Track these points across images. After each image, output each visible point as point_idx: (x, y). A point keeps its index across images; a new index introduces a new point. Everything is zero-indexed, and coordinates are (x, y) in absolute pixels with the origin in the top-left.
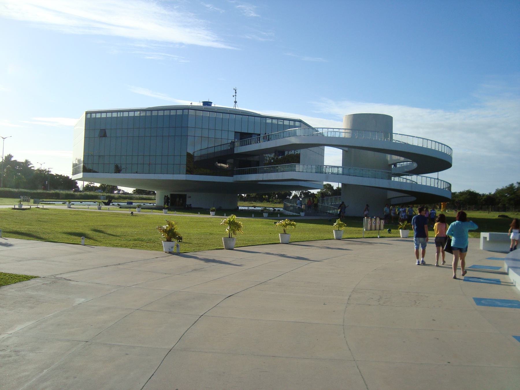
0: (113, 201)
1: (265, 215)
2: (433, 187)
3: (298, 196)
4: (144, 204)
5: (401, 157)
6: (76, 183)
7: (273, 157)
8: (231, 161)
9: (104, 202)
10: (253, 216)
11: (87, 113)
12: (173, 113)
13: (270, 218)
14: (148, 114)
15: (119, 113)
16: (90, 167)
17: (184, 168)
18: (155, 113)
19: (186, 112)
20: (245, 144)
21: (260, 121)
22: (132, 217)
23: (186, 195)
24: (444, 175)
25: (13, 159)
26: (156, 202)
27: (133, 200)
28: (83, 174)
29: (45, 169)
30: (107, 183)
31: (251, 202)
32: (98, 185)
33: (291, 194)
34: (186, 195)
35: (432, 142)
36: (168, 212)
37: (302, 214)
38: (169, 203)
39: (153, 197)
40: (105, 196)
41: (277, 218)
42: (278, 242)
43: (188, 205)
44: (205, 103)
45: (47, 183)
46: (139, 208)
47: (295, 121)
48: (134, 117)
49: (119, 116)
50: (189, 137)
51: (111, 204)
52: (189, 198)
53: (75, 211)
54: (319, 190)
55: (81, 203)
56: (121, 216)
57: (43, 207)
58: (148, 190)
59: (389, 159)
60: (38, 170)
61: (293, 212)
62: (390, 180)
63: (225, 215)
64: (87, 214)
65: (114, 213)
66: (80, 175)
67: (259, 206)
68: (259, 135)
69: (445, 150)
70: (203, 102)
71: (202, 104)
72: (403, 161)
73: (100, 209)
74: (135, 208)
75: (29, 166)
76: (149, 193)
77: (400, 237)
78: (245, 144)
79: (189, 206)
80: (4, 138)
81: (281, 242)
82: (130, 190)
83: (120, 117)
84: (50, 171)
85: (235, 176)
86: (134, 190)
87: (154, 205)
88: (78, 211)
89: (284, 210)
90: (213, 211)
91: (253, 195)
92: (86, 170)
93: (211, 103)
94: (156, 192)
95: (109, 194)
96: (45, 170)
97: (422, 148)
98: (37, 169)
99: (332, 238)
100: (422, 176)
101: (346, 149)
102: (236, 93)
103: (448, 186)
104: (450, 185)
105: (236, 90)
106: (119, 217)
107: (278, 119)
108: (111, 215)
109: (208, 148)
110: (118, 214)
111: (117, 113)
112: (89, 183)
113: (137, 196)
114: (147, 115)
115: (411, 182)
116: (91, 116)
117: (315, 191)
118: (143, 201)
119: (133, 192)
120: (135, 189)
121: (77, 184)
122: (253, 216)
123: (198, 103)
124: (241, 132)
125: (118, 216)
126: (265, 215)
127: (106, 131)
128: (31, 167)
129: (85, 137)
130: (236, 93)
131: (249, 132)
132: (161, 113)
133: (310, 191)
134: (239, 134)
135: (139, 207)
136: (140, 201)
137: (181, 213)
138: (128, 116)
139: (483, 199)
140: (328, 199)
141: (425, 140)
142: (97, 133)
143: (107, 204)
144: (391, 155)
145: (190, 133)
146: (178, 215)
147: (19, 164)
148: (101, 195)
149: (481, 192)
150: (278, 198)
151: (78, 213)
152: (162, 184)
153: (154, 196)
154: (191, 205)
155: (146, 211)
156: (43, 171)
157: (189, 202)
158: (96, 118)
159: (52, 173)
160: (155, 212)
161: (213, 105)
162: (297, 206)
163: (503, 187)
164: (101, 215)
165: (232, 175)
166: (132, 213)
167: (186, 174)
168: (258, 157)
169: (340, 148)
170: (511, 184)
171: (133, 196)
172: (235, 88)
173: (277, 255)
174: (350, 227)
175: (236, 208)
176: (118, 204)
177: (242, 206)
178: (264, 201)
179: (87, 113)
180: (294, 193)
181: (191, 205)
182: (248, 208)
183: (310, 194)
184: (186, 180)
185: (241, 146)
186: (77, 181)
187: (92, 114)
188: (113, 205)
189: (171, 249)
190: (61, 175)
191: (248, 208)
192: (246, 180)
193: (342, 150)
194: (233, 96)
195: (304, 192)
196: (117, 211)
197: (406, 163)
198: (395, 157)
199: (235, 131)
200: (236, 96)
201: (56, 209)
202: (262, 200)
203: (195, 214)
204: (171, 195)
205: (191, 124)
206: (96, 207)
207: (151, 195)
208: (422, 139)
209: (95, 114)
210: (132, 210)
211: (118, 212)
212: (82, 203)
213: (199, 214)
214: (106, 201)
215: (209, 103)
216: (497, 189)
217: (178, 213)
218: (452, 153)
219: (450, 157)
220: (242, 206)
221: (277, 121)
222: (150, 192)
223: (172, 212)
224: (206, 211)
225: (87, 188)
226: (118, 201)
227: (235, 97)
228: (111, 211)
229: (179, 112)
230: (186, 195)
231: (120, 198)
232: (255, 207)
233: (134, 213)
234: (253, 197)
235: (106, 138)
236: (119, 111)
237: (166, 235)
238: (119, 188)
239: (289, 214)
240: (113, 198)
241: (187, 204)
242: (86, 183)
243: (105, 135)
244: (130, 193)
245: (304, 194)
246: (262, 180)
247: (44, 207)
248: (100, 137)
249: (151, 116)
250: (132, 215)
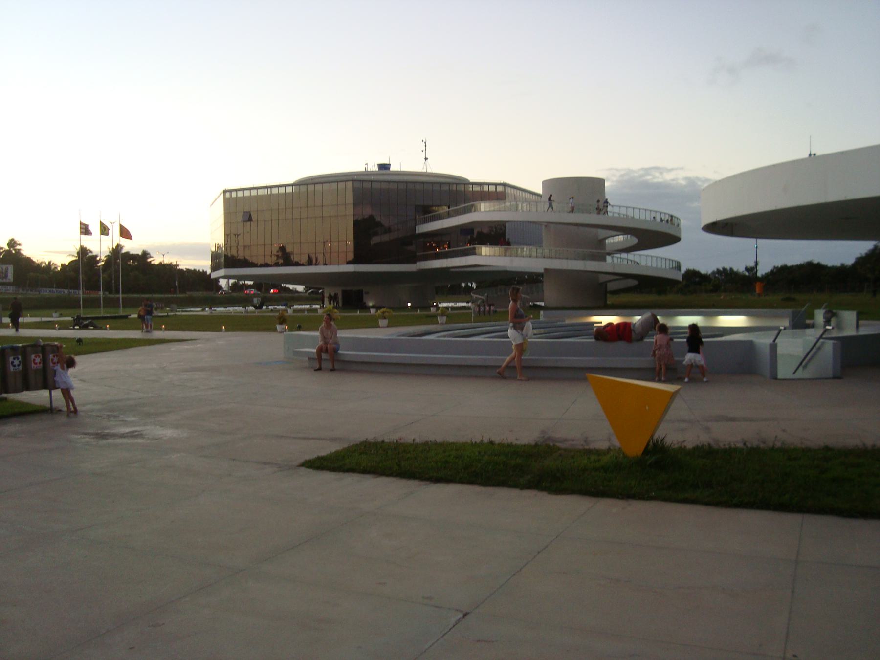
11: (225, 192)
25: (124, 251)
66: (222, 272)
75: (149, 260)
80: (113, 222)
85: (418, 263)
102: (426, 146)
105: (425, 143)
115: (619, 262)
116: (231, 195)
127: (252, 214)
128: (150, 262)
129: (225, 223)
130: (426, 146)
144: (20, 326)
147: (134, 257)
149: (830, 264)
159: (181, 267)
161: (392, 168)
163: (861, 254)
172: (424, 140)
215: (70, 401)
225: (235, 288)
243: (250, 219)
248: (244, 222)
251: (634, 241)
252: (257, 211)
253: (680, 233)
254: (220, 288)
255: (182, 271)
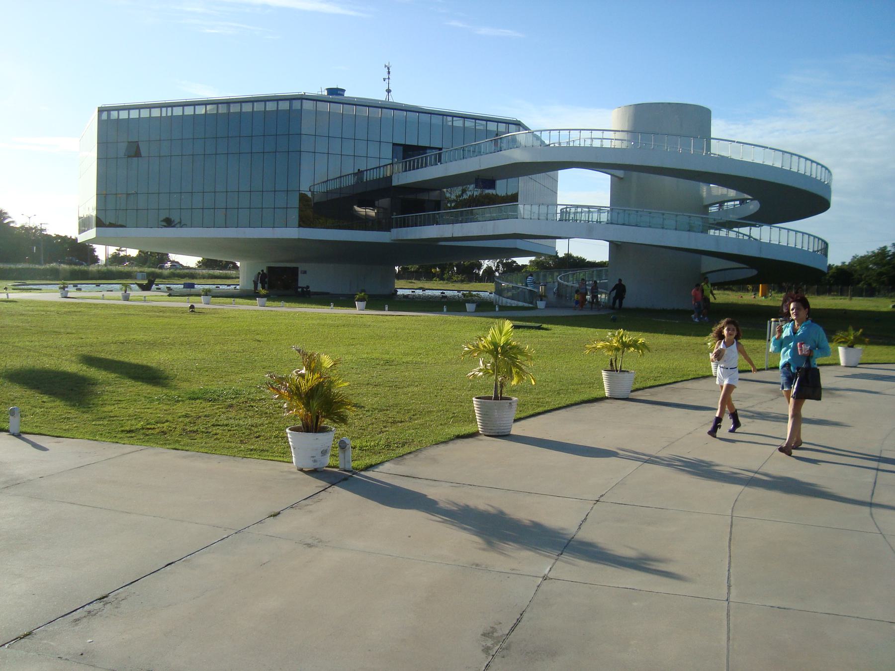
0: (157, 281)
1: (470, 307)
2: (800, 249)
3: (494, 269)
4: (216, 287)
5: (730, 190)
6: (93, 250)
7: (455, 198)
8: (385, 202)
9: (139, 285)
10: (445, 310)
11: (101, 111)
12: (271, 106)
13: (481, 314)
14: (222, 109)
15: (164, 110)
16: (111, 219)
17: (294, 215)
18: (234, 109)
19: (296, 105)
20: (414, 165)
21: (441, 123)
22: (193, 317)
23: (297, 268)
24: (811, 225)
26: (240, 283)
27: (196, 278)
28: (96, 230)
29: (35, 226)
30: (149, 250)
31: (410, 281)
32: (133, 253)
33: (479, 266)
34: (297, 268)
35: (791, 156)
36: (268, 303)
37: (541, 304)
38: (266, 285)
39: (233, 273)
40: (145, 274)
41: (492, 314)
42: (596, 394)
43: (302, 288)
44: (331, 91)
45: (35, 251)
46: (206, 295)
47: (509, 123)
48: (195, 116)
49: (164, 114)
50: (303, 154)
51: (154, 287)
52: (304, 273)
53: (73, 304)
54: (533, 258)
55: (97, 286)
56: (168, 314)
57: (8, 297)
58: (225, 259)
59: (705, 194)
60: (23, 227)
61: (519, 301)
62: (706, 235)
63: (387, 308)
64: (94, 311)
65: (155, 306)
67: (433, 289)
68: (440, 149)
69: (816, 173)
70: (327, 89)
71: (325, 93)
72: (734, 198)
73: (126, 298)
74: (200, 295)
75: (6, 221)
76: (225, 266)
77: (838, 364)
78: (414, 165)
79: (305, 289)
81: (607, 395)
82: (190, 261)
83: (167, 116)
84: (45, 230)
86: (199, 262)
87: (236, 287)
88: (79, 303)
89: (498, 296)
90: (360, 300)
91: (413, 268)
92: (100, 223)
93: (343, 91)
94: (238, 264)
95: (153, 269)
96: (36, 227)
97: (781, 170)
98: (20, 226)
99: (701, 373)
100: (780, 228)
101: (620, 173)
102: (389, 73)
103: (823, 247)
104: (826, 244)
105: (389, 69)
106: (162, 317)
107: (476, 119)
108: (147, 311)
109: (341, 177)
110: (163, 310)
111: (160, 109)
112: (117, 250)
113: (205, 272)
114: (220, 112)
116: (109, 115)
117: (522, 261)
118: (215, 280)
119: (197, 265)
120: (200, 259)
121: (95, 251)
122: (445, 310)
123: (317, 87)
124: (404, 143)
125: (161, 314)
126: (470, 307)
127: (141, 145)
128: (9, 223)
129: (99, 159)
130: (389, 73)
131: (421, 144)
132: (247, 108)
133: (514, 259)
134: (401, 148)
135: (207, 293)
136: (210, 281)
137: (293, 305)
138: (181, 114)
139: (830, 274)
140: (568, 276)
141: (788, 154)
142: (122, 148)
143: (146, 288)
145: (306, 145)
146: (289, 310)
148: (138, 270)
150: (458, 273)
151: (76, 310)
152: (248, 248)
153: (234, 272)
154: (308, 287)
155: (223, 301)
156: (31, 228)
157: (303, 281)
158: (118, 120)
159: (49, 232)
160: (239, 304)
161: (346, 94)
162: (527, 288)
164: (125, 314)
165: (387, 228)
166: (192, 307)
167: (300, 226)
168: (437, 192)
169: (601, 170)
170: (882, 246)
171: (197, 271)
172: (387, 64)
173: (670, 463)
174: (656, 335)
175: (393, 292)
176: (167, 288)
177: (404, 289)
178: (435, 279)
179: (101, 111)
180: (486, 263)
181: (308, 287)
182: (412, 292)
183: (515, 264)
184: (299, 240)
185: (406, 171)
186: (95, 246)
187: (112, 112)
188: (157, 289)
189: (318, 457)
190: (66, 236)
191: (412, 292)
192: (418, 238)
193: (609, 176)
194: (384, 80)
195: (504, 261)
196: (163, 303)
197: (732, 203)
198: (717, 190)
199: (394, 142)
200: (389, 78)
201: (32, 301)
202: (430, 277)
203: (323, 307)
204: (269, 268)
205: (307, 126)
206: (120, 294)
207: (230, 269)
208: (781, 153)
209: (117, 112)
210: (192, 298)
211: (163, 306)
212: (99, 286)
213: (332, 306)
214: (145, 282)
216: (854, 255)
217: (287, 304)
218: (831, 180)
219: (828, 188)
220: (404, 289)
221: (474, 124)
222: (228, 263)
223: (276, 303)
224: (347, 301)
225: (116, 259)
226: (169, 281)
227: (387, 80)
228: (149, 304)
229: (284, 106)
230: (297, 268)
231: (173, 276)
232: (424, 290)
233: (196, 305)
234: (414, 272)
235: (140, 158)
236: (163, 105)
237: (301, 410)
238: (173, 257)
239: (508, 305)
240: (160, 276)
241: (300, 285)
242: (112, 250)
243: (138, 154)
244: (191, 266)
245: (504, 265)
246: (451, 236)
247: (9, 297)
248: (129, 157)
249: (229, 113)
250: (192, 311)
251: (753, 206)
252: (148, 209)
253: (830, 197)
254: (96, 260)
255: (49, 236)
